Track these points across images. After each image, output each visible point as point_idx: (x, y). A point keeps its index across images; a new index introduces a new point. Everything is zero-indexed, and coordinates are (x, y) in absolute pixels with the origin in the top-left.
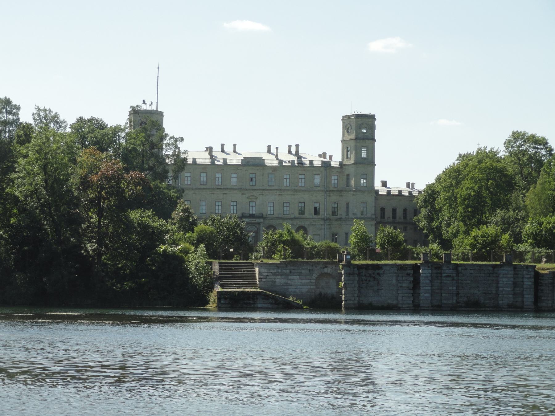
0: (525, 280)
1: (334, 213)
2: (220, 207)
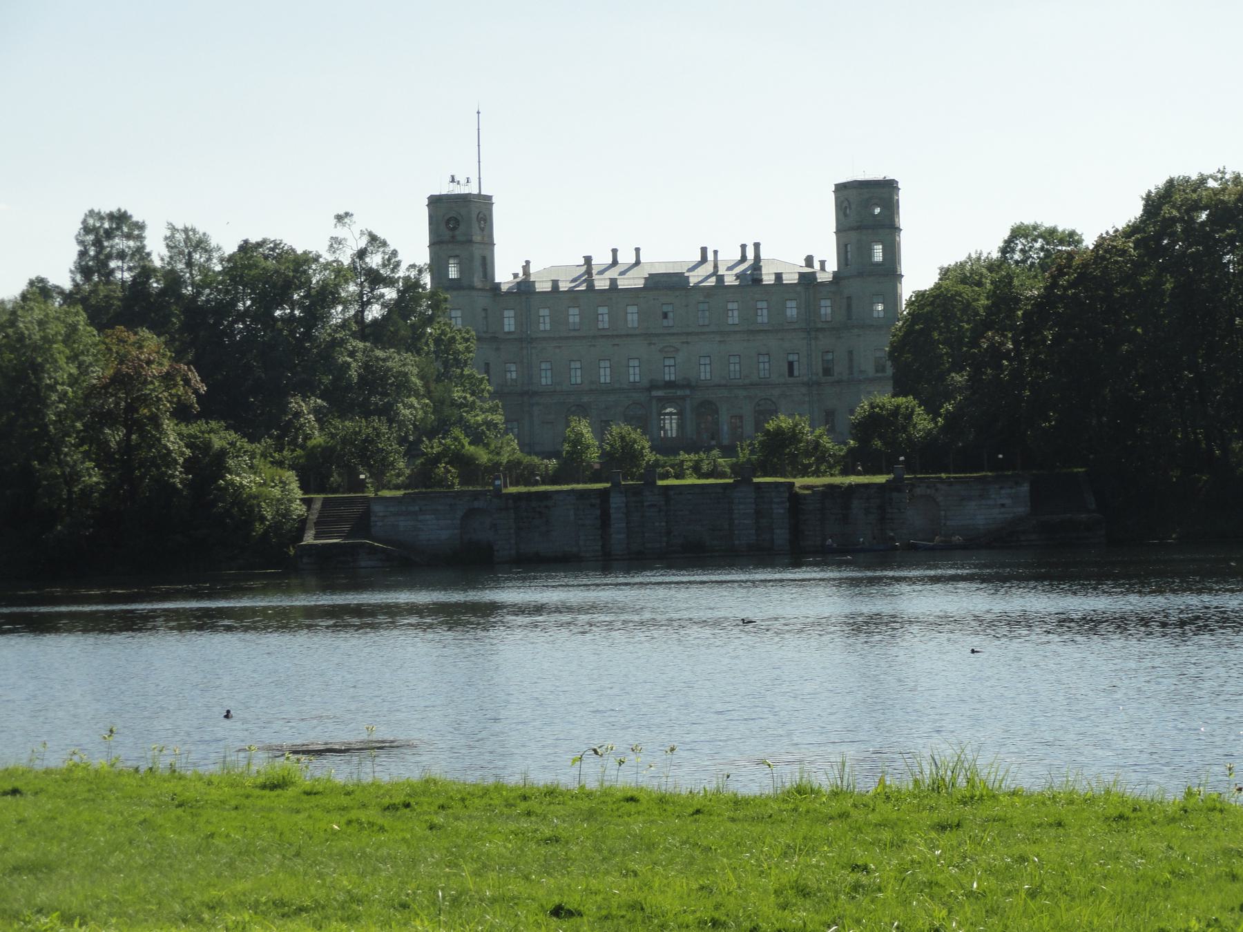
0: (775, 506)
1: (827, 371)
2: (608, 370)
